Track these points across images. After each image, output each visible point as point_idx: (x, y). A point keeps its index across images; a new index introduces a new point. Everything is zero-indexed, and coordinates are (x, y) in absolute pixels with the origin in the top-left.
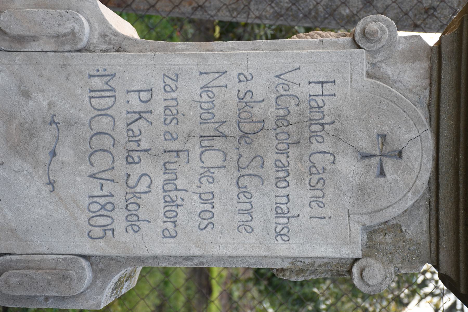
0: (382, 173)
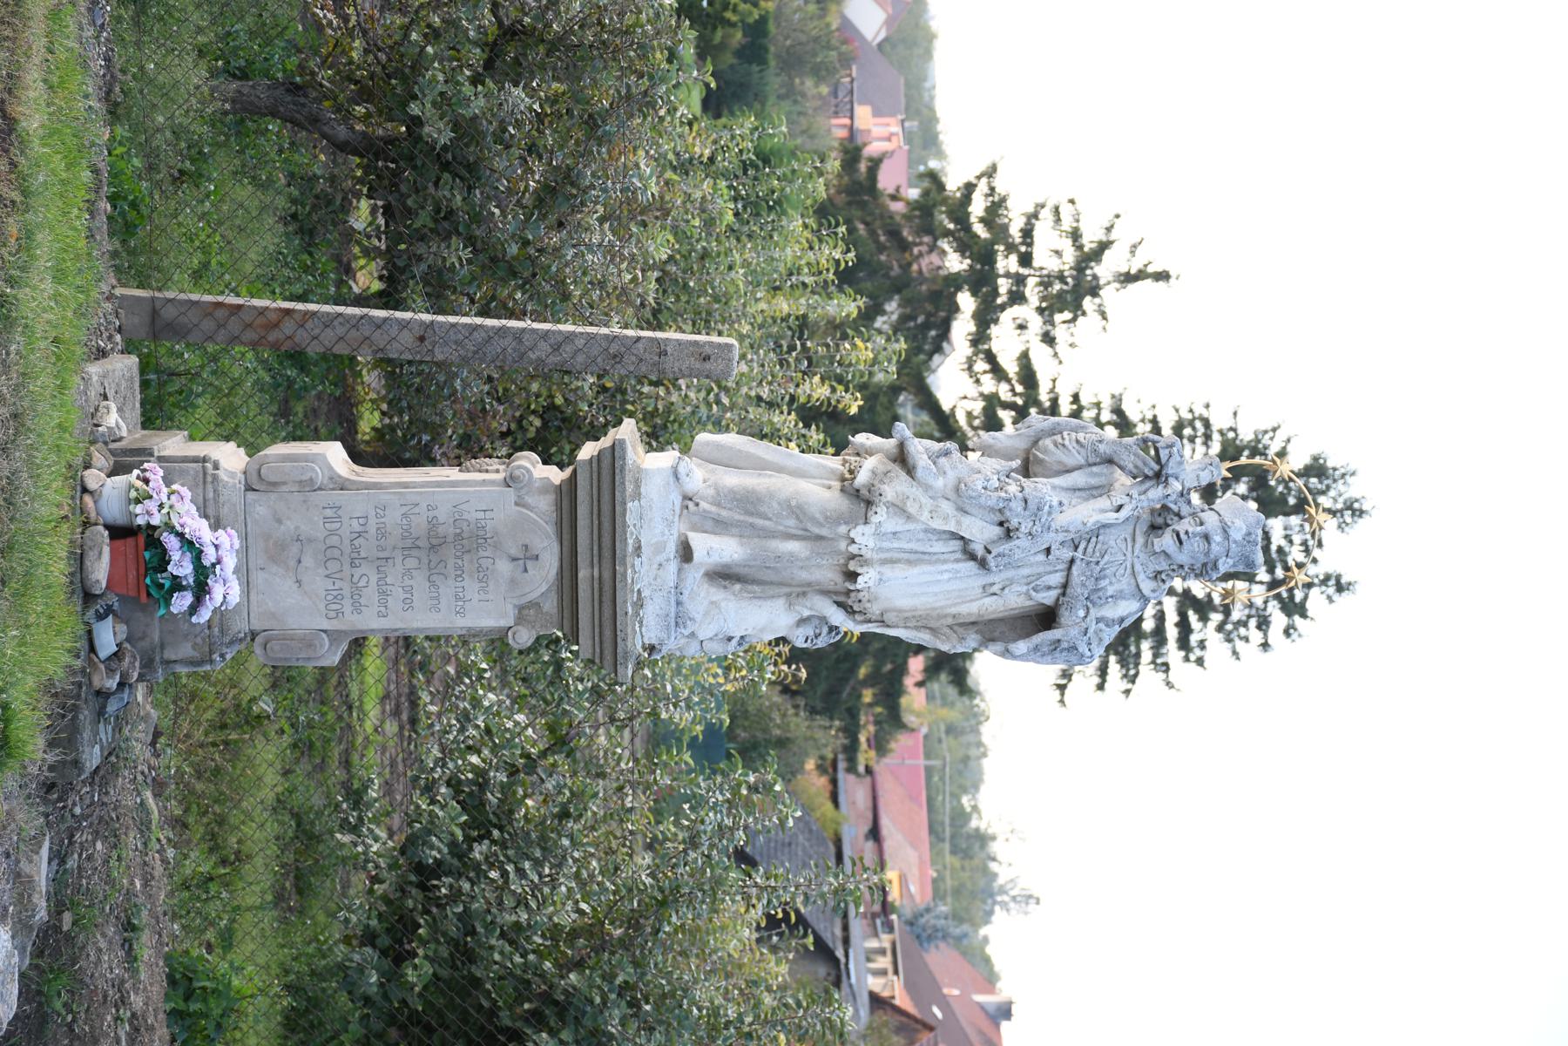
0: (526, 570)
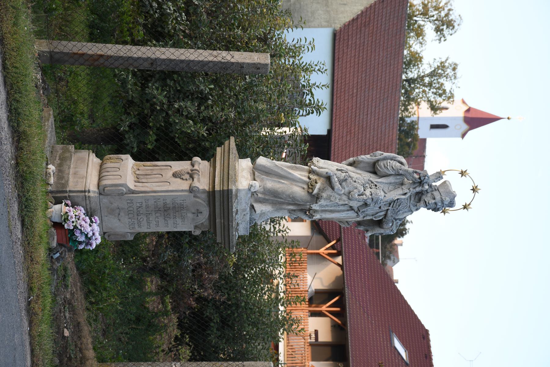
0: (198, 216)
